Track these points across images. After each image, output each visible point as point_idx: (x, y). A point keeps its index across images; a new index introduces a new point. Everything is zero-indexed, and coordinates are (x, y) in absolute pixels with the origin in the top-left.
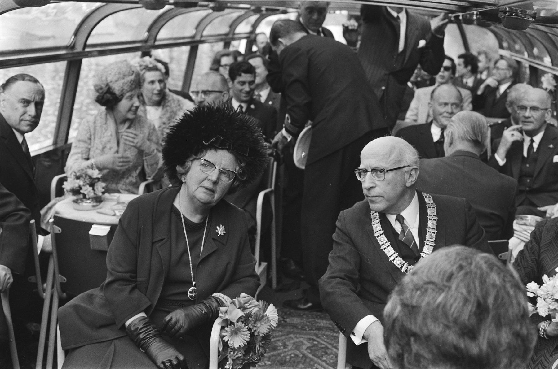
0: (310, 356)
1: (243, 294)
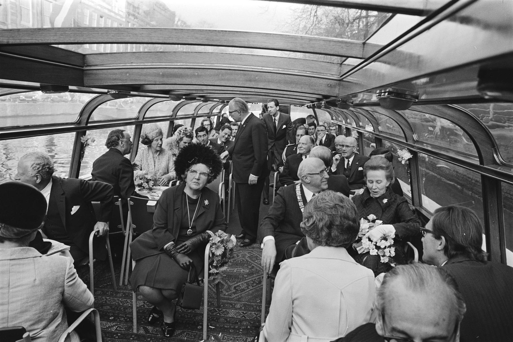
0: (250, 260)
1: (220, 231)
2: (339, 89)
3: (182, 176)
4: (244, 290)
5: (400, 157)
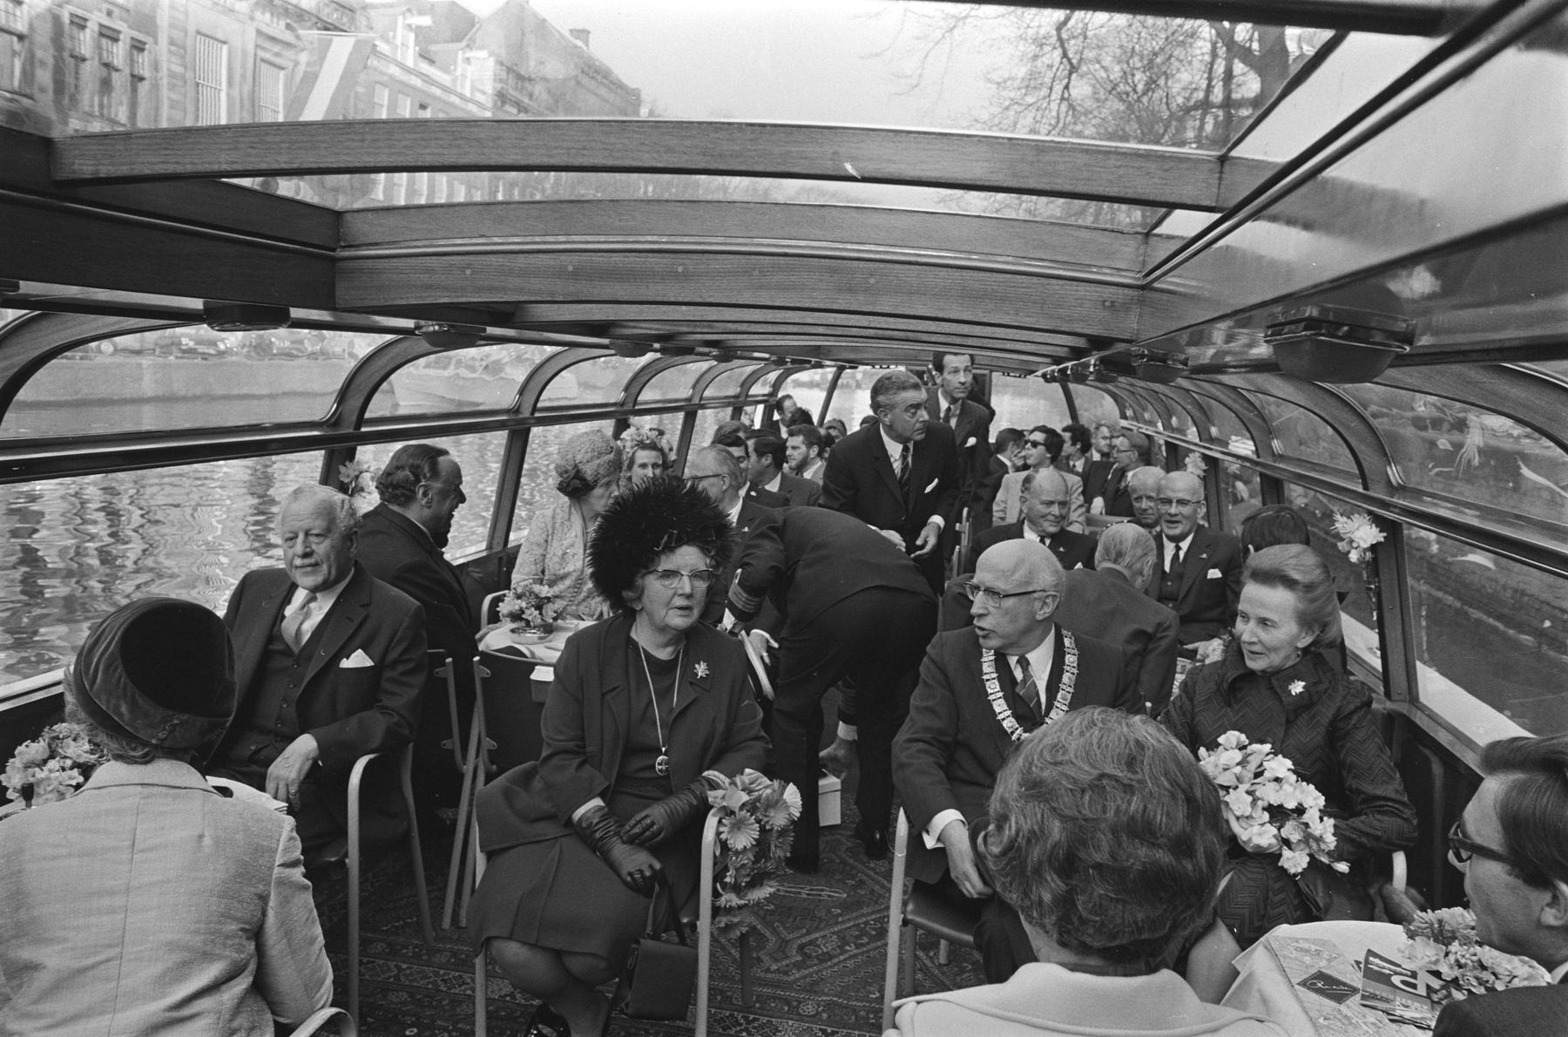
0: (851, 861)
1: (748, 771)
2: (1141, 315)
3: (627, 594)
4: (831, 957)
5: (1343, 540)
